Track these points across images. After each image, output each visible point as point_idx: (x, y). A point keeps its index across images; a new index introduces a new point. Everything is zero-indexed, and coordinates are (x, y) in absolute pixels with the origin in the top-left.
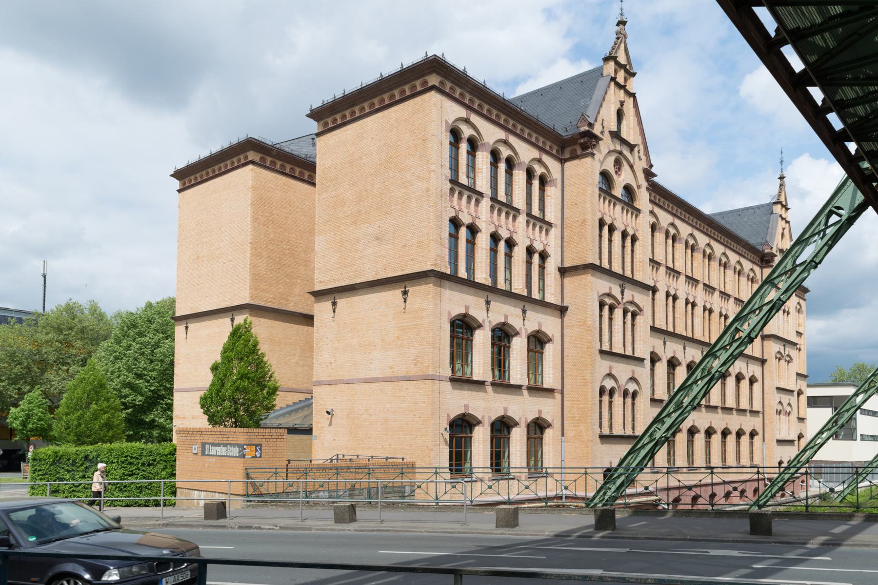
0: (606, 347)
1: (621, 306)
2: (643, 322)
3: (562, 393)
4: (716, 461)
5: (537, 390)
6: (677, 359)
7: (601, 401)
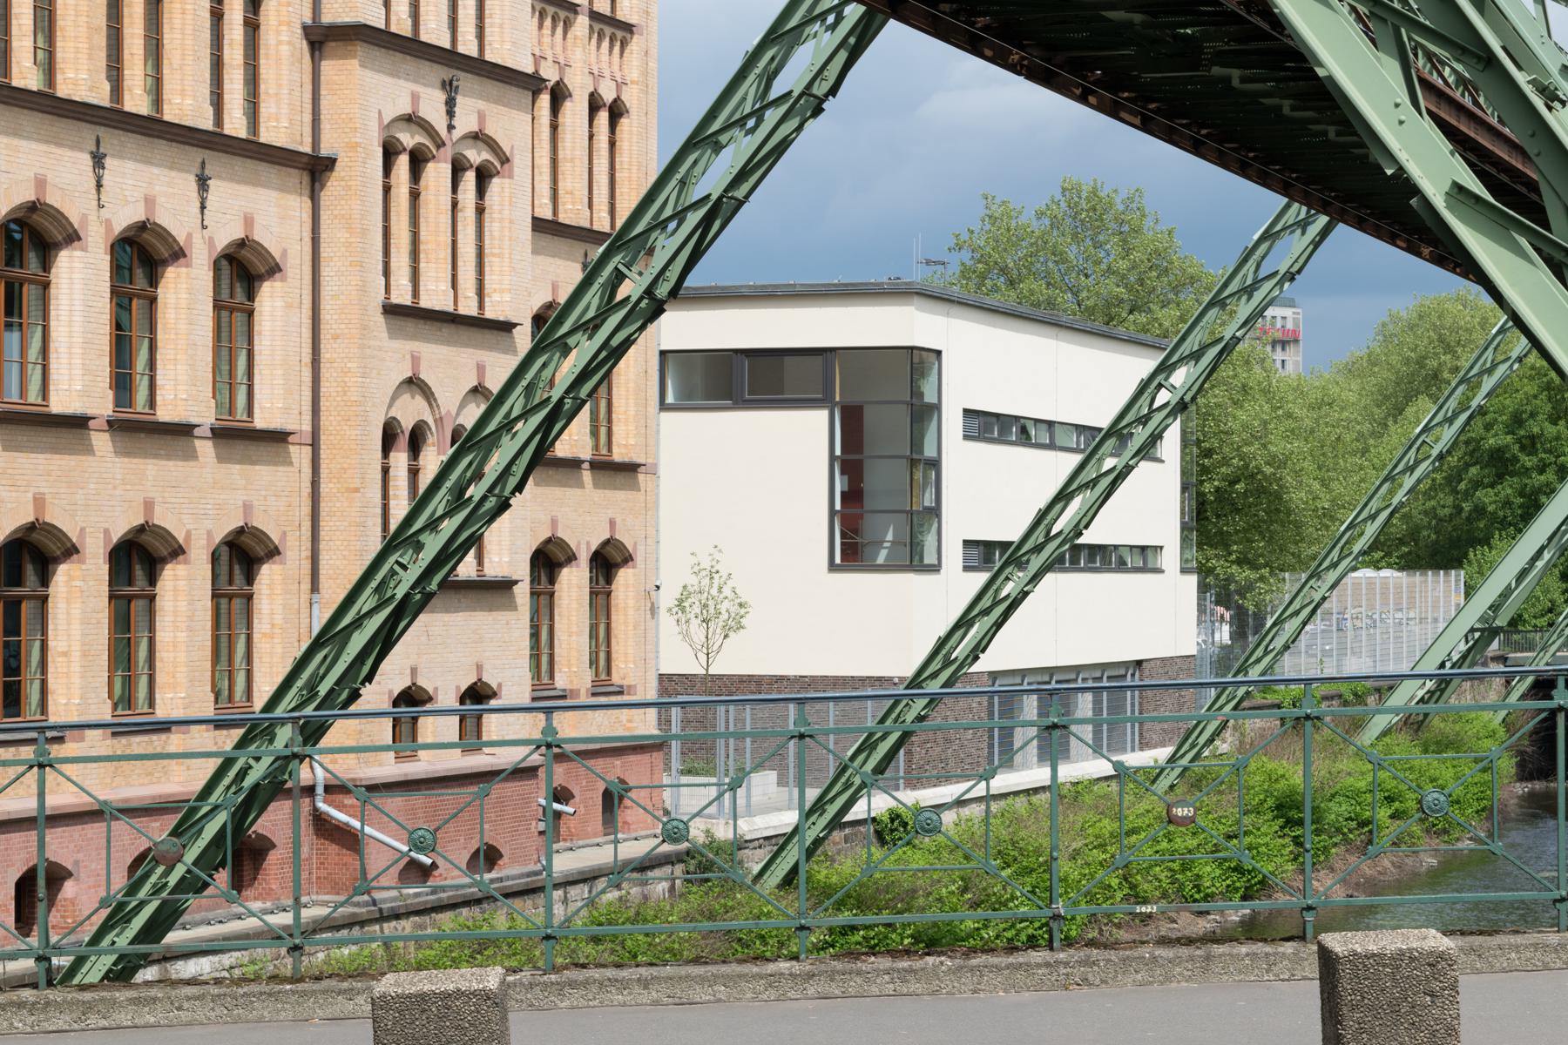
0: (401, 296)
1: (448, 152)
2: (513, 203)
3: (315, 445)
4: (573, 671)
5: (241, 437)
6: (163, 235)
7: (386, 471)
